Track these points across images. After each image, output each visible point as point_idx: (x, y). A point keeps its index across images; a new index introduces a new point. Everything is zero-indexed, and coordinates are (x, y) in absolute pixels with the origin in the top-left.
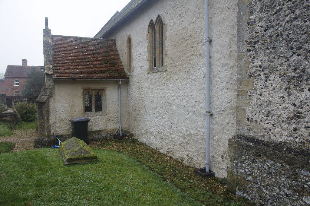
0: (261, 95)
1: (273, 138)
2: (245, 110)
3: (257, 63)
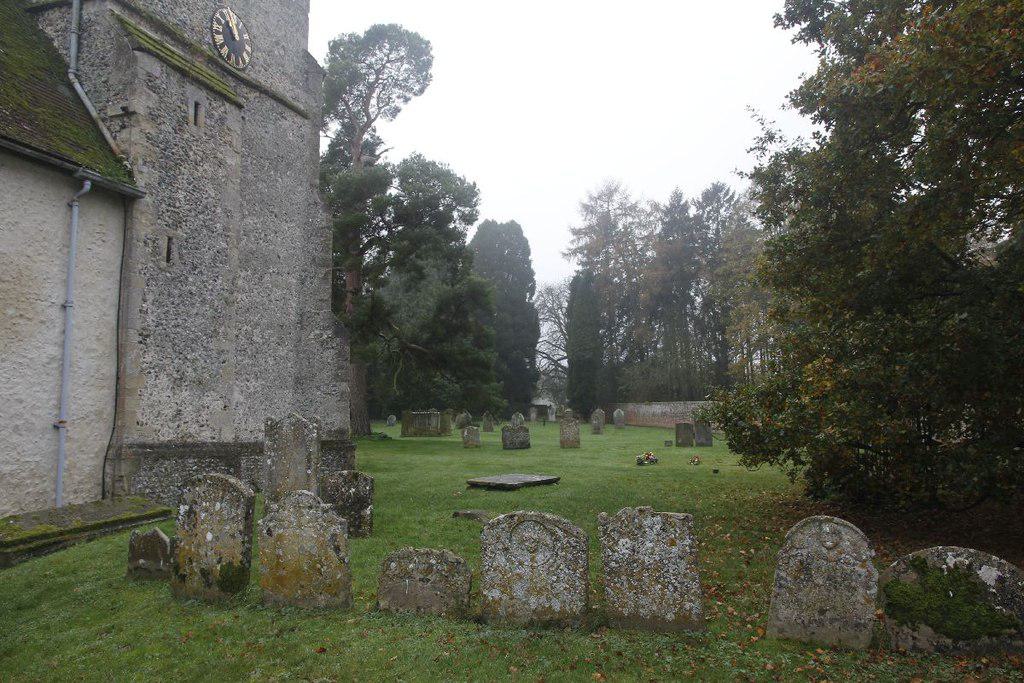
0: (151, 395)
1: (162, 438)
2: (135, 412)
3: (148, 358)
